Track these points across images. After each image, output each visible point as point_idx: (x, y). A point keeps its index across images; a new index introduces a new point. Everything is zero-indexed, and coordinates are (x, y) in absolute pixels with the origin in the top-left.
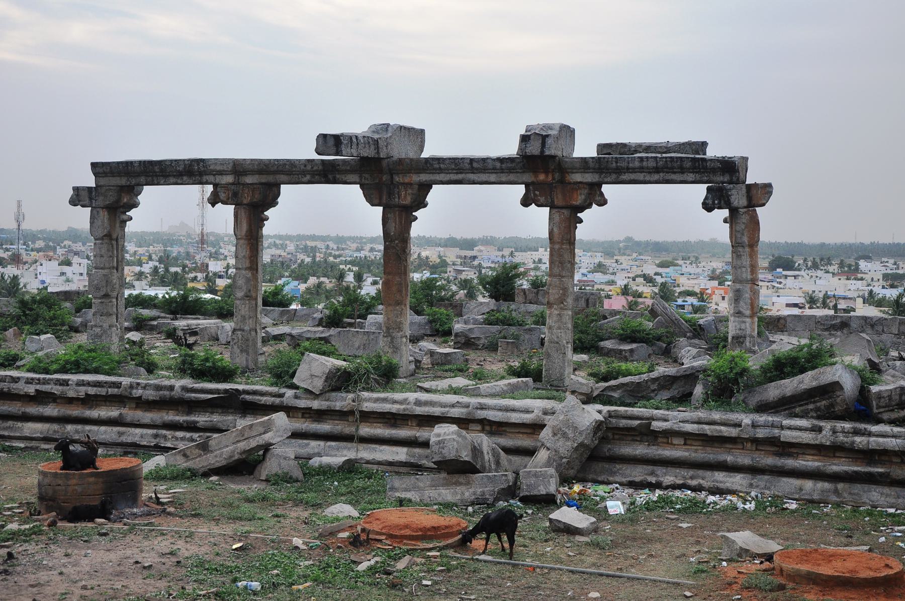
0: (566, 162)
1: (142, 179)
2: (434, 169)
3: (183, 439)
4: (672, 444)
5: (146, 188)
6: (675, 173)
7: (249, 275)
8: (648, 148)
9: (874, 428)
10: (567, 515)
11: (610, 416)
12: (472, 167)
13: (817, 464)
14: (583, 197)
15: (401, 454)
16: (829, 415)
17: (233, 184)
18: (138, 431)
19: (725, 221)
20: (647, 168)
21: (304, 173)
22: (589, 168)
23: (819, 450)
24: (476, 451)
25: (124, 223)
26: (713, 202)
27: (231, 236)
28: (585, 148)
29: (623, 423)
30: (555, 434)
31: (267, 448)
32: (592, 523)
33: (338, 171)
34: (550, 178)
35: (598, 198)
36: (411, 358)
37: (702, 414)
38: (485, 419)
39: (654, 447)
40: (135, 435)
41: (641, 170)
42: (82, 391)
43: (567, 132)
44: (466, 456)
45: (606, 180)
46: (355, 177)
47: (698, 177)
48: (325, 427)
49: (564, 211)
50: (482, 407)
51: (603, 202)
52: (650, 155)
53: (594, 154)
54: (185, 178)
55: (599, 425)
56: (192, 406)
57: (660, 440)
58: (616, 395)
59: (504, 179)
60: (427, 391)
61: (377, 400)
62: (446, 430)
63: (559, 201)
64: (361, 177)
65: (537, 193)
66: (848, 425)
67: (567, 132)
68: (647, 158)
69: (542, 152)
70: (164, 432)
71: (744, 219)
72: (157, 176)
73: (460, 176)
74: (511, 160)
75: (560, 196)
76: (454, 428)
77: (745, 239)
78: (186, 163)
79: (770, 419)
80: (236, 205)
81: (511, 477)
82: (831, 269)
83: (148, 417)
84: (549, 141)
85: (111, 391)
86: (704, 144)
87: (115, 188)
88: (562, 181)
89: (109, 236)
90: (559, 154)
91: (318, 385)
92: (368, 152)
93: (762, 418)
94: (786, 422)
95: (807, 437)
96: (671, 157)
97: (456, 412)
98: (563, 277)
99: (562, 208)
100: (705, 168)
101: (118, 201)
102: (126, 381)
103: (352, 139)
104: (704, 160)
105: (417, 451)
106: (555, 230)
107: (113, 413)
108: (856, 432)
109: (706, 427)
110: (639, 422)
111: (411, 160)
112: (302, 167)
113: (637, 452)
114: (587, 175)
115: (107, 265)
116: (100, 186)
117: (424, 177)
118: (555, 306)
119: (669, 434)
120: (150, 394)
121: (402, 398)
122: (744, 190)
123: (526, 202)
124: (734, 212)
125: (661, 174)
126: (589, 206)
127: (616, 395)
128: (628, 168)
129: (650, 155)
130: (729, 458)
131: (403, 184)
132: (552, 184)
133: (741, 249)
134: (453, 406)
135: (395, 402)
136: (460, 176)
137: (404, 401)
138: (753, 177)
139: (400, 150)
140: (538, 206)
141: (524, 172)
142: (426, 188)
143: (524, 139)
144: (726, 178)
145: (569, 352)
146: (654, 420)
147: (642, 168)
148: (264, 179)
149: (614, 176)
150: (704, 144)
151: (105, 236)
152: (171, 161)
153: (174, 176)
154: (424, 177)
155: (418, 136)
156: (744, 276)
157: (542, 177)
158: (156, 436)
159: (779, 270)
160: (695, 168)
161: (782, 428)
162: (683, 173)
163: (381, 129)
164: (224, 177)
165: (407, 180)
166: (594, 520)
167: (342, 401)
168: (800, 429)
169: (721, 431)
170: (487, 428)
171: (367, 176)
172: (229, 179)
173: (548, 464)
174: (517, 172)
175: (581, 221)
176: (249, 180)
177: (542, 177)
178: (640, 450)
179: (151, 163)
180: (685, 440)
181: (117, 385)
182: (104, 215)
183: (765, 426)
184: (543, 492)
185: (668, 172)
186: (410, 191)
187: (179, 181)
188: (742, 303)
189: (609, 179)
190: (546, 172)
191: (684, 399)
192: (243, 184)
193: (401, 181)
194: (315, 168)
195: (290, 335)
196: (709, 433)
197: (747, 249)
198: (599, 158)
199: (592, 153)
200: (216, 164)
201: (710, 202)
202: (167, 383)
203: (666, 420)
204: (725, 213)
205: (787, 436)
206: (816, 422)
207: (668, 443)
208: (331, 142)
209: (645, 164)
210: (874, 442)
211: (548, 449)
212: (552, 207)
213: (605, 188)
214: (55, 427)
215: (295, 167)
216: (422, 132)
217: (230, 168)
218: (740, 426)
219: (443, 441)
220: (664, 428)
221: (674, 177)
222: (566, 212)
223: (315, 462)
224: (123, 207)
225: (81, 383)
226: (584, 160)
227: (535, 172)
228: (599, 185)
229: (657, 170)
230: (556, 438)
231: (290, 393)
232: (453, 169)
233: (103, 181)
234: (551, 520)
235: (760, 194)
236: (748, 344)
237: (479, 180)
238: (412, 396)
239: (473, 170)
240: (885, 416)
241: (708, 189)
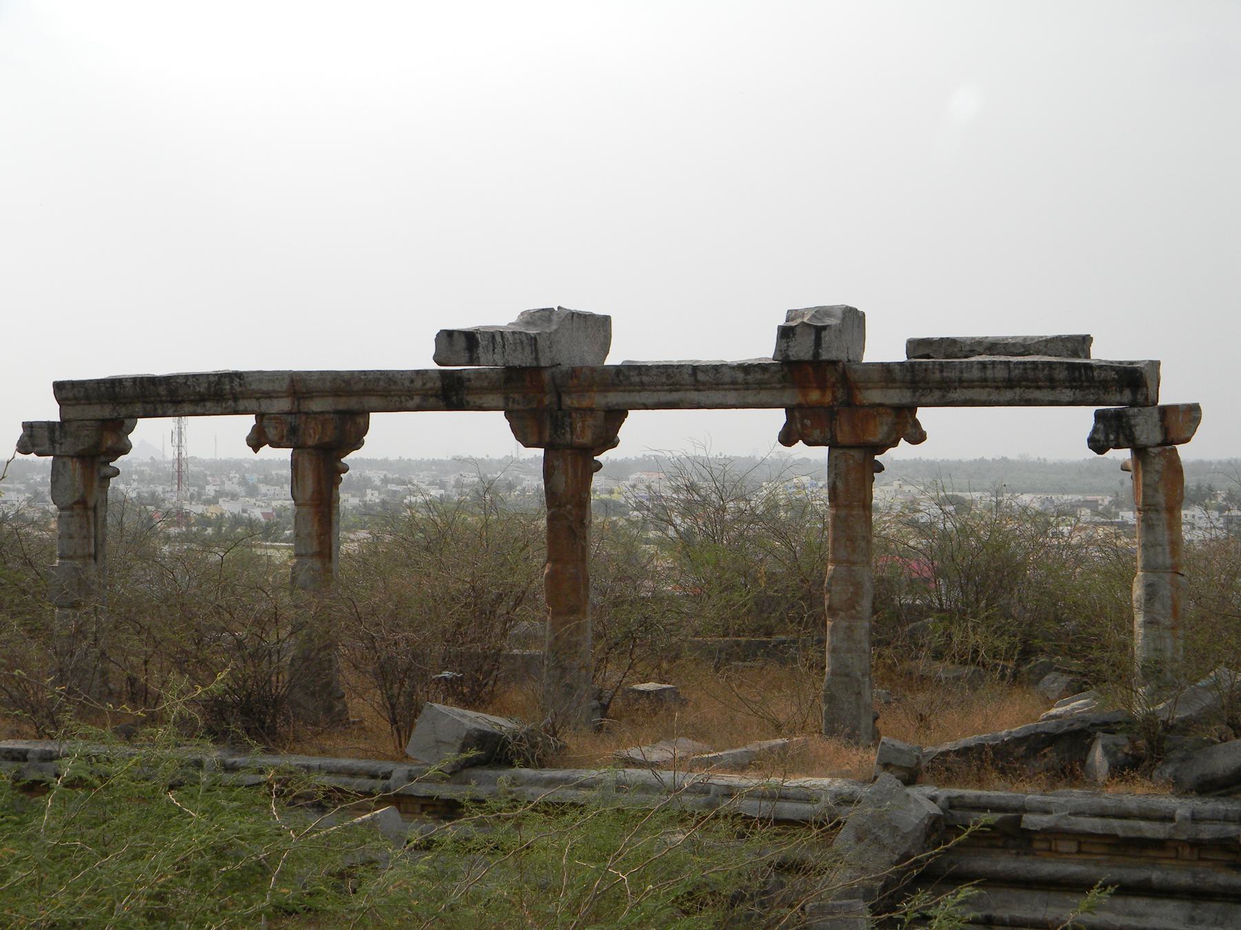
0: (856, 371)
1: (138, 407)
2: (631, 384)
4: (1056, 852)
5: (141, 422)
6: (1039, 388)
7: (317, 564)
8: (993, 346)
11: (952, 807)
12: (697, 381)
14: (885, 428)
17: (290, 413)
20: (994, 380)
21: (410, 394)
22: (894, 381)
25: (106, 479)
26: (1107, 436)
27: (278, 482)
28: (884, 346)
30: (859, 839)
33: (468, 389)
34: (828, 398)
35: (909, 430)
39: (1026, 858)
41: (984, 383)
43: (854, 319)
45: (924, 400)
46: (498, 399)
47: (1079, 394)
49: (852, 452)
53: (902, 357)
54: (208, 404)
57: (1037, 845)
59: (750, 400)
63: (844, 435)
64: (507, 398)
65: (808, 422)
67: (854, 319)
69: (816, 354)
71: (1159, 464)
72: (161, 402)
73: (675, 396)
74: (762, 367)
75: (846, 428)
77: (1161, 498)
78: (212, 379)
79: (1221, 807)
80: (295, 448)
86: (1085, 341)
87: (93, 420)
88: (850, 403)
89: (82, 502)
90: (843, 356)
92: (521, 359)
98: (854, 563)
99: (851, 447)
100: (1091, 380)
101: (97, 445)
103: (495, 337)
104: (1089, 367)
106: (840, 485)
109: (1116, 823)
110: (999, 816)
111: (593, 370)
112: (407, 383)
113: (999, 867)
114: (891, 392)
115: (80, 552)
116: (69, 421)
117: (614, 398)
118: (842, 614)
122: (1156, 416)
123: (787, 438)
124: (1140, 452)
125: (1018, 390)
126: (895, 444)
128: (961, 381)
130: (1156, 876)
131: (577, 409)
132: (832, 407)
133: (1153, 515)
136: (675, 396)
139: (571, 354)
140: (809, 444)
141: (784, 388)
142: (616, 416)
143: (785, 333)
144: (1127, 395)
146: (1026, 811)
147: (985, 380)
148: (343, 404)
149: (937, 394)
150: (1085, 341)
151: (76, 503)
152: (187, 377)
153: (191, 401)
154: (614, 398)
155: (598, 327)
156: (1160, 560)
157: (814, 396)
160: (1074, 380)
162: (1053, 388)
163: (540, 318)
164: (275, 401)
165: (585, 403)
169: (1140, 830)
171: (517, 396)
172: (284, 405)
174: (772, 388)
175: (880, 468)
176: (316, 405)
177: (814, 396)
179: (153, 381)
180: (1080, 843)
182: (74, 469)
183: (1213, 819)
185: (1028, 387)
186: (590, 421)
187: (199, 410)
188: (1158, 606)
189: (928, 399)
190: (822, 387)
191: (1071, 770)
192: (306, 413)
193: (576, 405)
194: (429, 385)
196: (1120, 833)
197: (1164, 515)
198: (912, 364)
199: (899, 355)
200: (261, 381)
201: (1101, 436)
203: (1047, 812)
207: (1050, 850)
208: (461, 343)
209: (989, 373)
212: (833, 445)
213: (922, 414)
215: (395, 383)
216: (606, 320)
217: (285, 387)
218: (1172, 819)
220: (1045, 825)
221: (1037, 394)
222: (857, 454)
224: (106, 454)
226: (886, 368)
227: (803, 386)
228: (913, 410)
229: (1010, 384)
230: (862, 846)
232: (662, 384)
233: (73, 413)
235: (1184, 420)
237: (708, 402)
239: (698, 386)
241: (1098, 416)
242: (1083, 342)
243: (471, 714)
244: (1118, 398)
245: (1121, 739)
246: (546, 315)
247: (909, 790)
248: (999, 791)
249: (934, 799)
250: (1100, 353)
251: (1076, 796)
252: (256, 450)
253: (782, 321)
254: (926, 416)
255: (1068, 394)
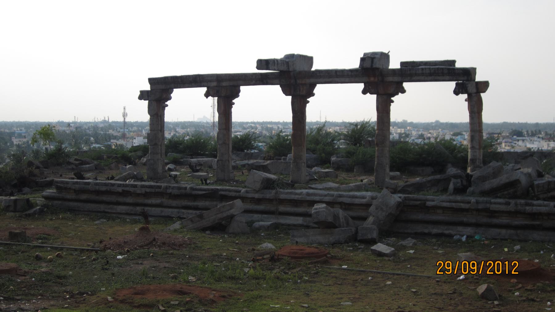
3: (191, 213)
5: (175, 90)
6: (439, 76)
9: (535, 202)
10: (380, 247)
13: (508, 221)
15: (299, 220)
16: (514, 196)
17: (217, 86)
18: (170, 210)
19: (466, 100)
23: (509, 213)
24: (336, 217)
28: (394, 64)
29: (412, 203)
30: (377, 209)
31: (232, 217)
32: (392, 251)
34: (376, 80)
36: (307, 174)
37: (451, 198)
38: (342, 202)
40: (167, 212)
41: (423, 74)
42: (143, 191)
44: (330, 219)
48: (261, 207)
50: (341, 196)
51: (403, 91)
52: (426, 67)
55: (399, 204)
56: (196, 197)
58: (410, 189)
60: (313, 188)
61: (287, 193)
62: (320, 206)
66: (523, 201)
67: (385, 57)
68: (425, 68)
69: (372, 66)
70: (183, 211)
73: (330, 80)
76: (324, 205)
77: (476, 110)
79: (485, 199)
81: (353, 229)
82: (541, 136)
83: (174, 203)
84: (375, 61)
85: (157, 190)
90: (381, 67)
91: (258, 186)
92: (284, 68)
93: (481, 199)
94: (493, 200)
95: (503, 208)
96: (438, 68)
97: (327, 199)
102: (163, 185)
105: (308, 219)
107: (158, 201)
108: (527, 204)
109: (454, 204)
110: (420, 202)
111: (306, 72)
117: (312, 80)
119: (435, 208)
120: (175, 192)
121: (302, 192)
122: (474, 84)
124: (470, 96)
126: (397, 94)
127: (410, 189)
129: (426, 67)
130: (465, 220)
134: (326, 196)
135: (296, 194)
137: (301, 194)
138: (479, 78)
139: (300, 67)
142: (313, 86)
143: (362, 60)
144: (465, 78)
145: (388, 169)
148: (232, 83)
154: (312, 80)
155: (309, 60)
157: (372, 79)
158: (179, 212)
159: (515, 137)
161: (491, 203)
162: (443, 76)
166: (393, 249)
167: (270, 194)
168: (500, 204)
170: (344, 207)
172: (214, 84)
173: (373, 223)
177: (372, 79)
178: (420, 216)
181: (160, 187)
184: (369, 237)
195: (248, 164)
199: (398, 67)
202: (184, 186)
203: (433, 201)
204: (465, 96)
205: (494, 207)
206: (507, 200)
209: (424, 71)
210: (535, 209)
211: (373, 216)
214: (131, 208)
216: (311, 58)
219: (318, 212)
221: (439, 78)
223: (257, 224)
225: (143, 186)
226: (394, 70)
231: (243, 190)
234: (372, 250)
235: (484, 86)
236: (478, 163)
238: (305, 191)
240: (541, 196)
241: (456, 84)
242: (453, 62)
243: (265, 173)
244: (463, 78)
245: (459, 180)
246: (292, 56)
247: (393, 195)
248: (420, 196)
249: (400, 197)
250: (457, 65)
251: (444, 197)
252: (207, 98)
253: (362, 56)
254: (406, 85)
255: (448, 77)
